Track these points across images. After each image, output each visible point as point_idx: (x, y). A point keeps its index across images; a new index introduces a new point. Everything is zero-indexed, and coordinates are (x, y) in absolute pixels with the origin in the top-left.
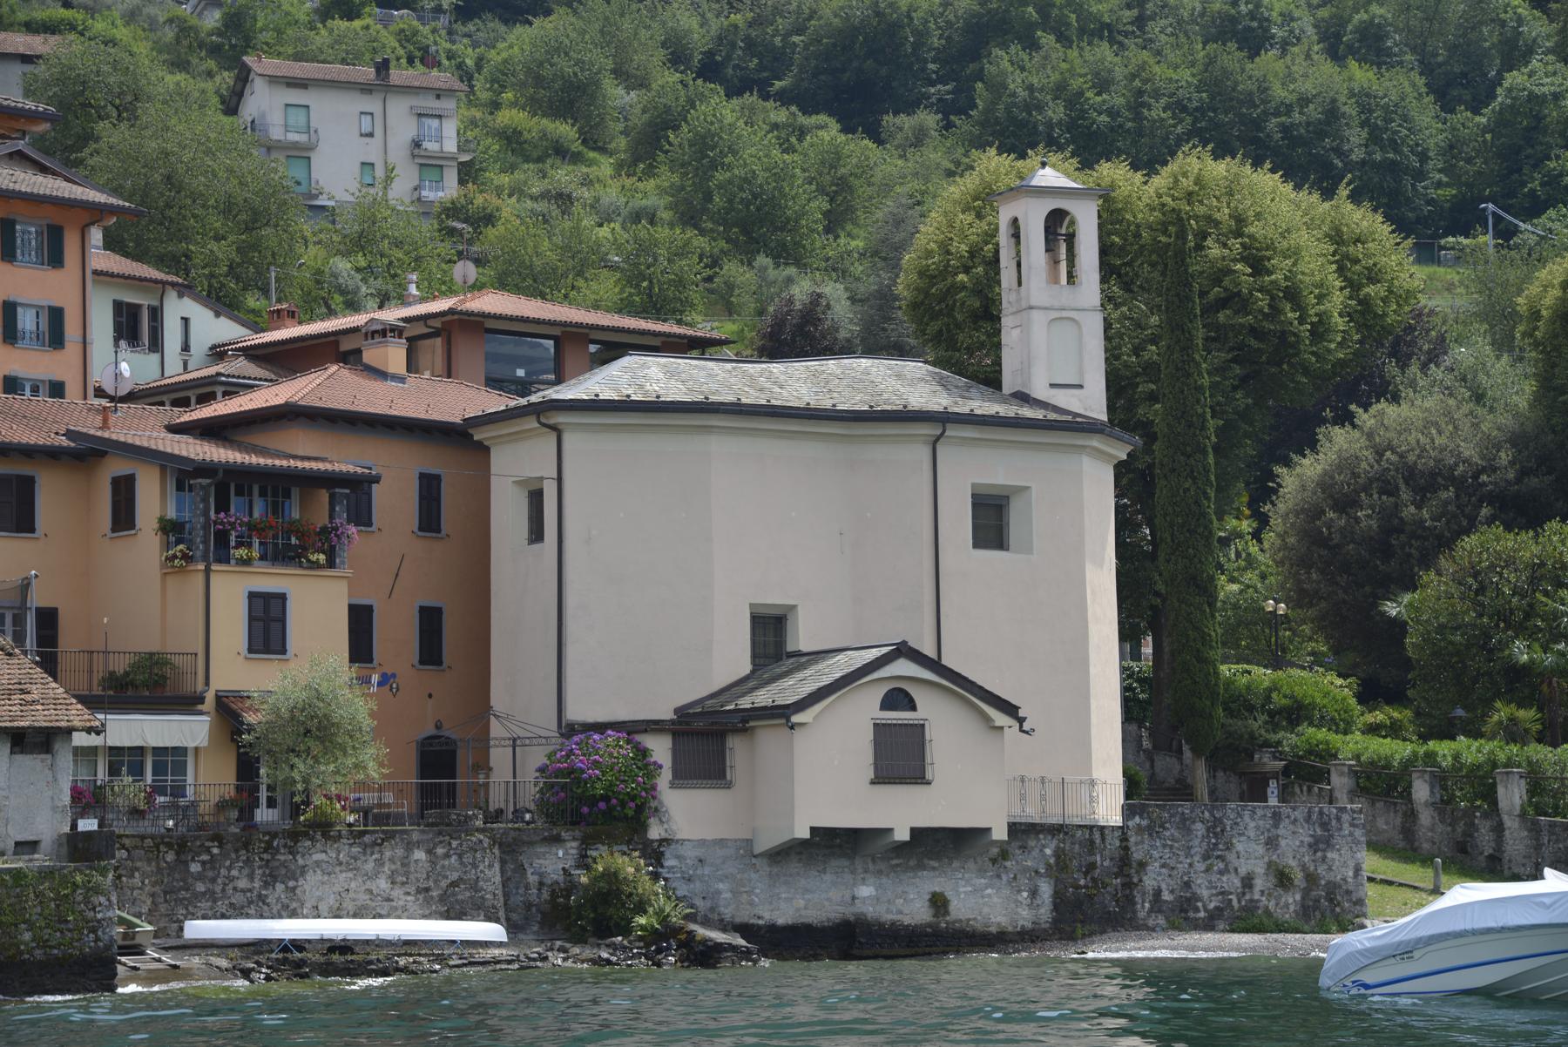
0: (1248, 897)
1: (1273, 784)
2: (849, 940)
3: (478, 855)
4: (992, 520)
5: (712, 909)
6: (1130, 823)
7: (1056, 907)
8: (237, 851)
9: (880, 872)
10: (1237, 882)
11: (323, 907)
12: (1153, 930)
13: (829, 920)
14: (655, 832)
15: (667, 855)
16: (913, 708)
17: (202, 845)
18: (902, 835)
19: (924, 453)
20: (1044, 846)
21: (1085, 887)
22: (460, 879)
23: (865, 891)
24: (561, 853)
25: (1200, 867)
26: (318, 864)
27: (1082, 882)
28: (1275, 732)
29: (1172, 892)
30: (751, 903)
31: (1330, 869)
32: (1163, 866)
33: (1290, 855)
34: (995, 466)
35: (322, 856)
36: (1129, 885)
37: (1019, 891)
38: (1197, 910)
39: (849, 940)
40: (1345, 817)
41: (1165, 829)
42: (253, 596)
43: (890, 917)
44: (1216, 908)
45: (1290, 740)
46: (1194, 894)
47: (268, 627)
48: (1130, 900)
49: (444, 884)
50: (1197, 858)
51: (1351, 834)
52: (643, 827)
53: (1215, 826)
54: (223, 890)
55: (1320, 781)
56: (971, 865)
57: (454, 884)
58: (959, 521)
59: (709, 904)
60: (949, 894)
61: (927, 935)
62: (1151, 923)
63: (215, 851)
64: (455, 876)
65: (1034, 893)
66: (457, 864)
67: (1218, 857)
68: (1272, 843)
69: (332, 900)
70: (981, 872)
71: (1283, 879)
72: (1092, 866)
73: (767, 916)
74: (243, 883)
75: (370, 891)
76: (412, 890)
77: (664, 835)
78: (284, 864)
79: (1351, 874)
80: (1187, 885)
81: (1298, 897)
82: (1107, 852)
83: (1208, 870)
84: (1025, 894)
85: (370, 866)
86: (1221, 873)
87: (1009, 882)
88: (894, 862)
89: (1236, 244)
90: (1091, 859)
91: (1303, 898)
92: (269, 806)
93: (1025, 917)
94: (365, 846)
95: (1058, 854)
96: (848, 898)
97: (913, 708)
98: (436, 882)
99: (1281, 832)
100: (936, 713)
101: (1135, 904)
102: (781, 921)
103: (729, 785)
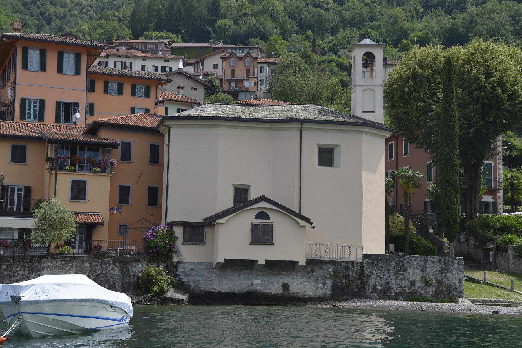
0: (413, 289)
1: (491, 253)
2: (250, 298)
3: (108, 265)
4: (326, 156)
5: (196, 286)
6: (364, 261)
8: (19, 262)
9: (263, 275)
10: (409, 283)
12: (372, 299)
13: (242, 291)
14: (175, 259)
15: (180, 267)
16: (269, 219)
17: (7, 260)
18: (262, 262)
19: (298, 133)
20: (329, 268)
21: (345, 283)
22: (101, 273)
23: (257, 282)
24: (140, 265)
25: (394, 277)
26: (49, 267)
27: (344, 281)
28: (495, 235)
29: (381, 286)
30: (212, 284)
31: (448, 280)
32: (378, 276)
34: (328, 138)
36: (363, 283)
37: (318, 284)
38: (391, 292)
39: (250, 298)
40: (455, 261)
41: (379, 263)
42: (73, 182)
43: (266, 291)
44: (399, 292)
45: (500, 239)
46: (390, 287)
47: (78, 191)
49: (95, 274)
50: (392, 274)
51: (458, 268)
53: (400, 263)
54: (14, 274)
55: (505, 252)
56: (299, 274)
57: (99, 275)
58: (312, 156)
59: (195, 284)
60: (290, 284)
61: (279, 297)
62: (371, 296)
63: (12, 261)
64: (99, 272)
65: (324, 284)
66: (100, 268)
67: (401, 274)
68: (423, 270)
70: (303, 276)
71: (427, 283)
73: (218, 289)
74: (21, 272)
77: (179, 260)
78: (36, 267)
79: (457, 282)
80: (387, 283)
81: (434, 289)
82: (354, 271)
83: (396, 279)
84: (321, 285)
85: (68, 268)
86: (402, 280)
89: (482, 69)
90: (348, 273)
91: (436, 290)
92: (79, 248)
93: (320, 292)
94: (67, 261)
95: (334, 271)
96: (250, 283)
97: (269, 219)
98: (92, 274)
100: (277, 221)
101: (366, 289)
102: (223, 291)
103: (204, 244)
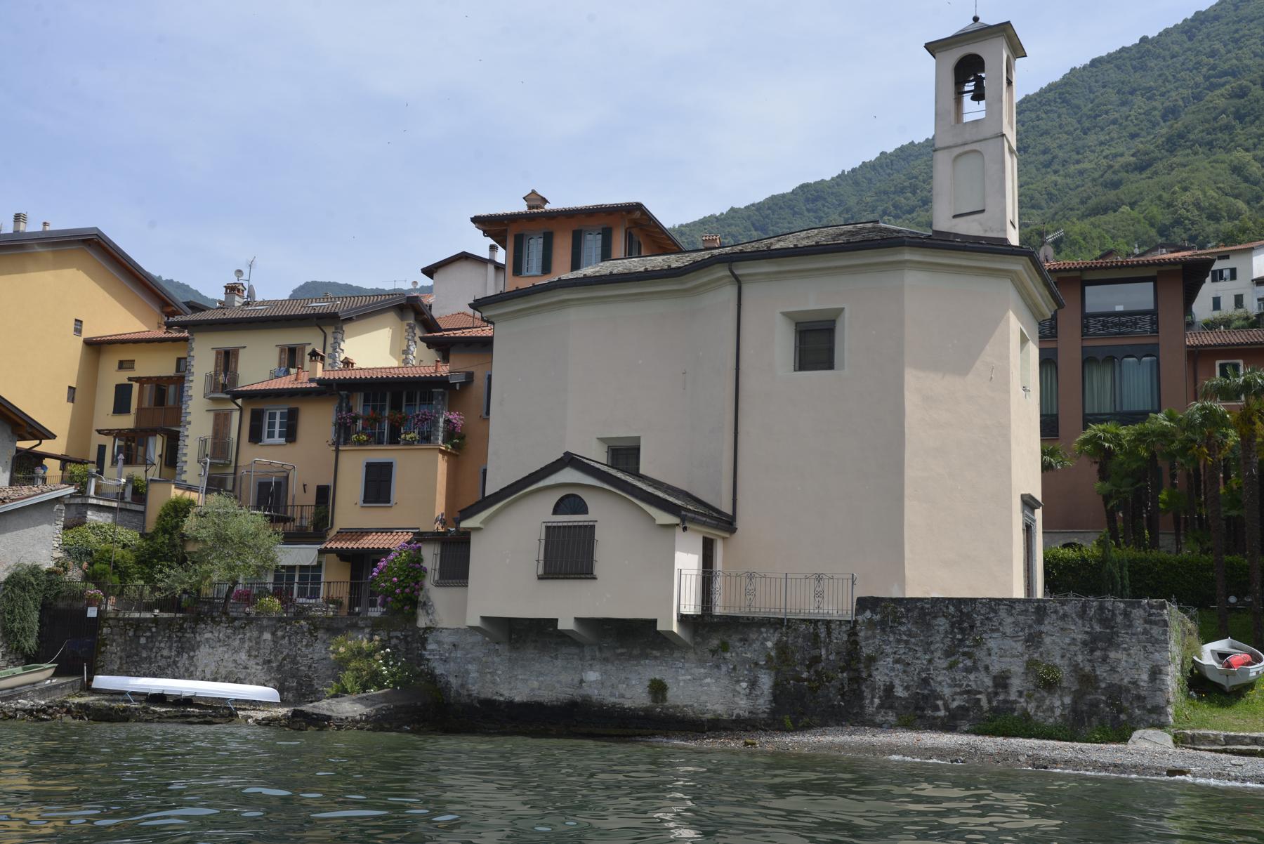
0: (1001, 697)
4: (816, 343)
5: (462, 686)
6: (860, 618)
7: (776, 698)
9: (606, 660)
10: (988, 682)
11: (208, 676)
13: (558, 700)
15: (430, 640)
20: (766, 639)
23: (592, 676)
25: (943, 663)
27: (805, 675)
29: (907, 688)
30: (494, 682)
31: (1113, 670)
32: (897, 661)
33: (1058, 653)
35: (208, 635)
36: (857, 680)
37: (738, 682)
38: (937, 708)
41: (901, 624)
42: (370, 467)
43: (613, 700)
44: (959, 707)
46: (933, 691)
48: (860, 696)
49: (280, 658)
50: (938, 654)
51: (1145, 632)
52: (413, 618)
53: (961, 622)
60: (669, 682)
65: (753, 684)
67: (964, 654)
68: (1033, 640)
69: (213, 667)
70: (701, 662)
72: (817, 659)
74: (165, 653)
75: (235, 661)
76: (260, 661)
77: (429, 624)
79: (1145, 677)
80: (926, 682)
81: (1067, 700)
82: (832, 647)
83: (951, 667)
84: (744, 685)
86: (968, 670)
87: (728, 673)
88: (619, 651)
90: (816, 652)
91: (1075, 702)
93: (742, 706)
94: (235, 628)
95: (782, 648)
98: (276, 656)
99: (1044, 628)
101: (862, 698)
102: (517, 699)
